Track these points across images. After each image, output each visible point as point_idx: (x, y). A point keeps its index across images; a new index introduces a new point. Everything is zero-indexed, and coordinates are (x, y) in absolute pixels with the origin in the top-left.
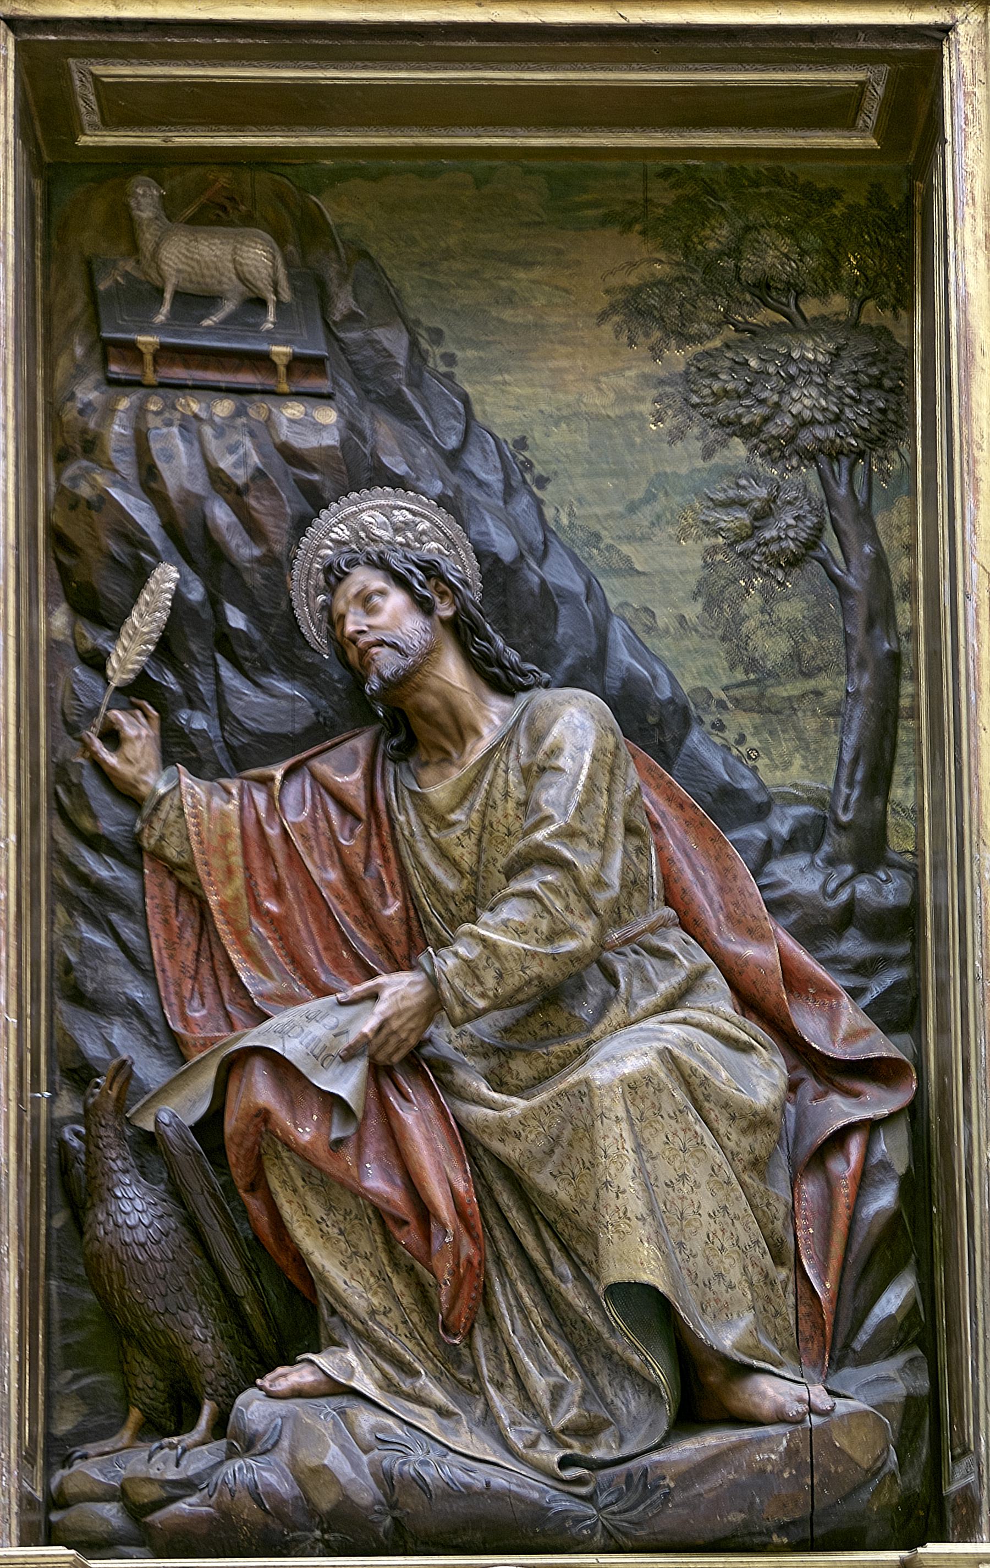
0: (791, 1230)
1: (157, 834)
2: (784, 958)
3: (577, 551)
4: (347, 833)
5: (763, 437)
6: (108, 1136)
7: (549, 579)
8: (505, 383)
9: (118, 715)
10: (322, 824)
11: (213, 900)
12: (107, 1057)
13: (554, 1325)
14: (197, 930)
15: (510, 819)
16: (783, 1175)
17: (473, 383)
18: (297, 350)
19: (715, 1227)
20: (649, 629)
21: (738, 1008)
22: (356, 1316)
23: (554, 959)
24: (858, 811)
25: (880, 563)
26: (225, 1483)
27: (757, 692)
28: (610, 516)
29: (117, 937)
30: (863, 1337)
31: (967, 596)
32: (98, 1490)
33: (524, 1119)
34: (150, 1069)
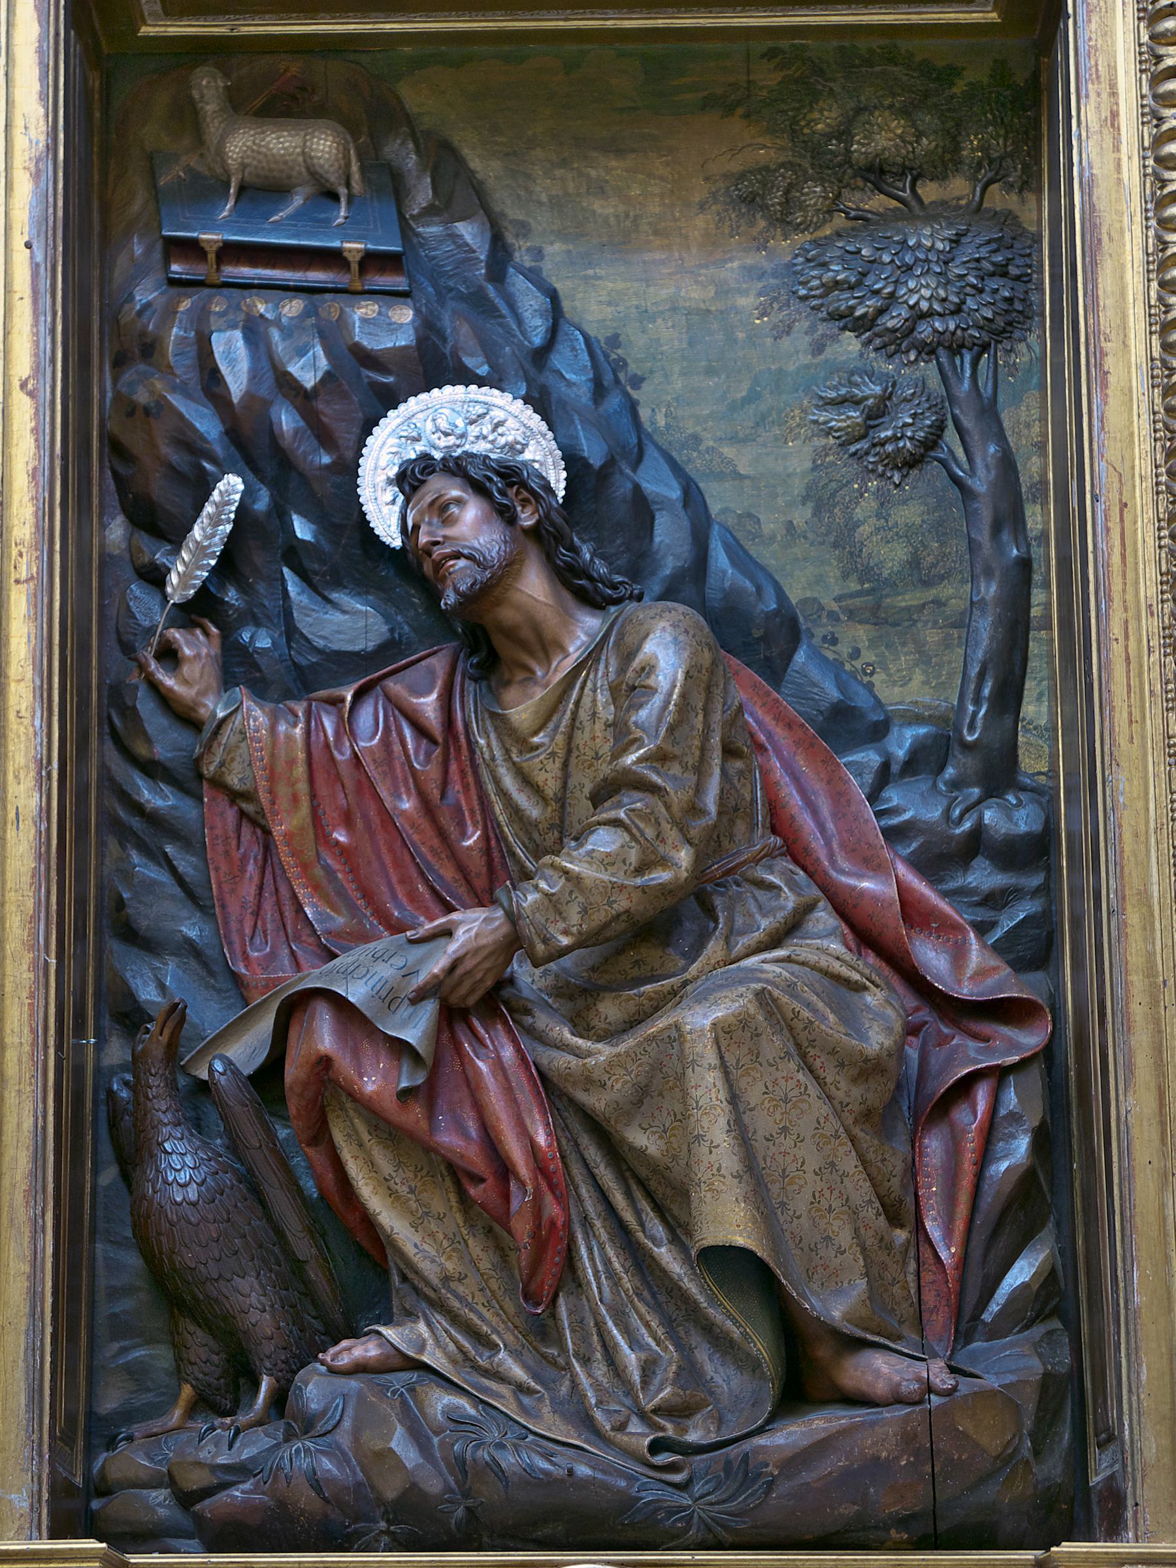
0: (912, 1190)
2: (902, 888)
3: (674, 454)
5: (876, 329)
6: (156, 1083)
7: (645, 485)
9: (176, 634)
10: (397, 748)
11: (278, 831)
13: (646, 1294)
14: (260, 863)
15: (598, 740)
16: (902, 1130)
18: (370, 246)
19: (820, 1185)
21: (852, 945)
22: (427, 1283)
23: (644, 892)
24: (985, 728)
25: (1008, 465)
29: (173, 870)
30: (994, 1307)
31: (1095, 498)
32: (143, 1475)
33: (610, 1065)
34: (207, 1013)
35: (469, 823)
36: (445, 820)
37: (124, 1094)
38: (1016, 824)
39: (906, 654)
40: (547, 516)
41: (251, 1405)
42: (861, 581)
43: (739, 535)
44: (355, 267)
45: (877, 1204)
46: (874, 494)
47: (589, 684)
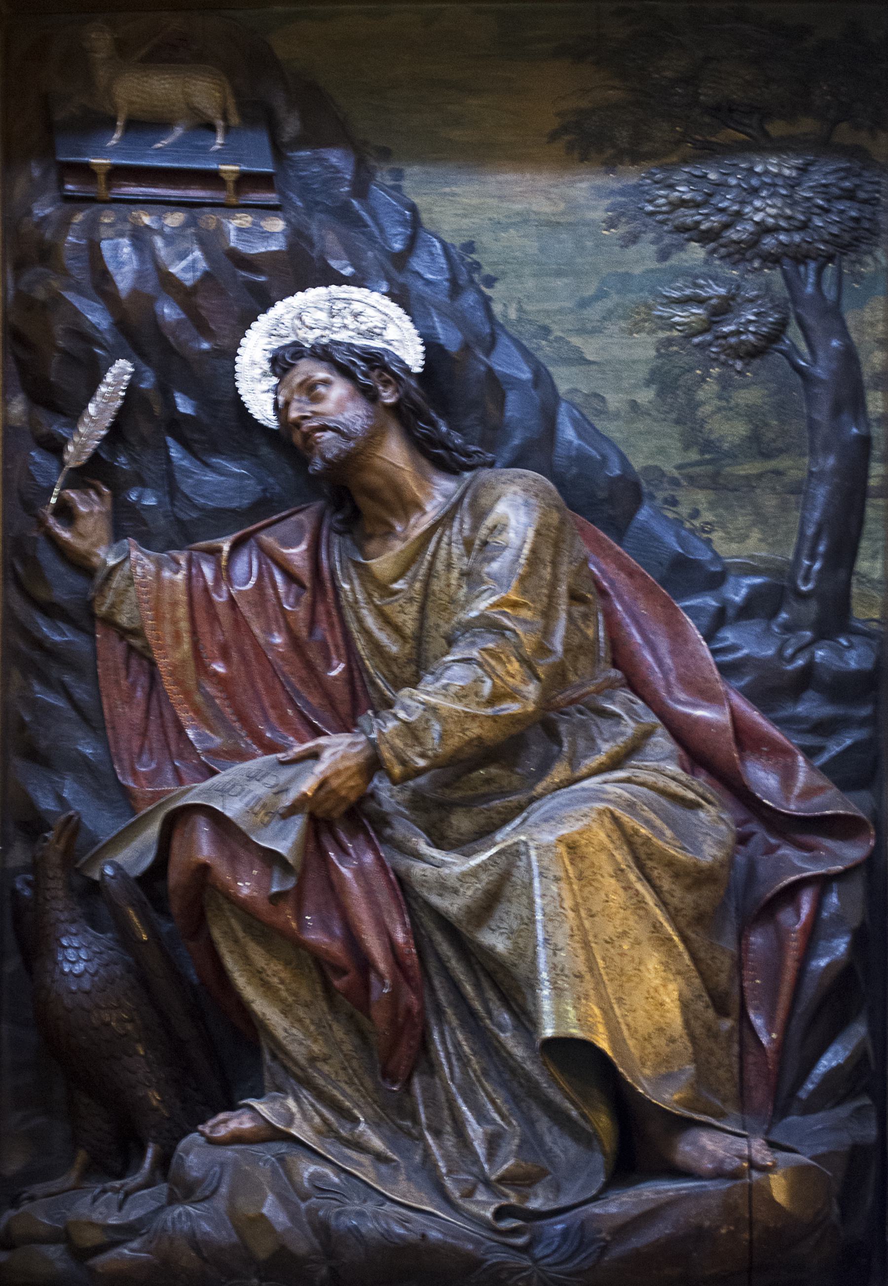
0: (737, 982)
1: (108, 601)
3: (524, 342)
4: (291, 600)
5: (722, 241)
6: (56, 886)
8: (454, 195)
9: (72, 494)
10: (270, 591)
11: (163, 664)
12: (58, 809)
13: (493, 1073)
15: (453, 587)
17: (418, 194)
20: (599, 413)
21: (687, 765)
25: (849, 357)
26: (164, 1230)
27: (713, 471)
28: (560, 311)
34: (100, 822)
35: (334, 656)
36: (313, 655)
37: (27, 893)
38: (847, 663)
39: (743, 515)
40: (407, 395)
41: (139, 1167)
42: (702, 452)
43: (585, 411)
44: (231, 185)
45: (707, 999)
46: (716, 378)
47: (445, 539)
